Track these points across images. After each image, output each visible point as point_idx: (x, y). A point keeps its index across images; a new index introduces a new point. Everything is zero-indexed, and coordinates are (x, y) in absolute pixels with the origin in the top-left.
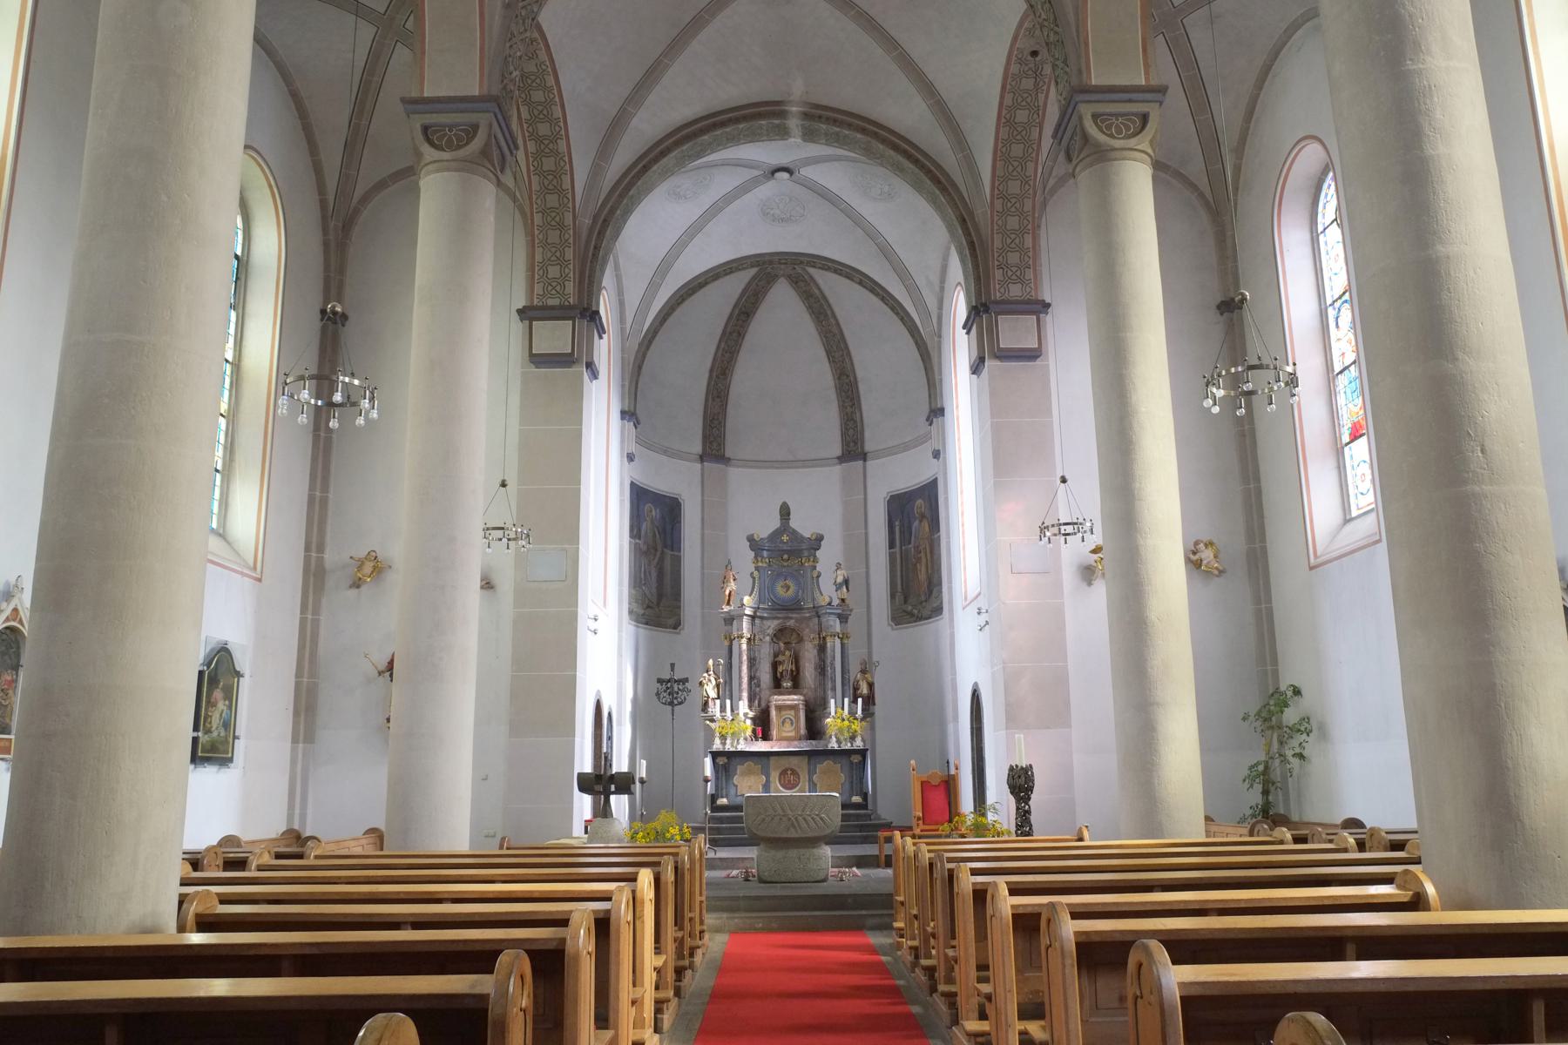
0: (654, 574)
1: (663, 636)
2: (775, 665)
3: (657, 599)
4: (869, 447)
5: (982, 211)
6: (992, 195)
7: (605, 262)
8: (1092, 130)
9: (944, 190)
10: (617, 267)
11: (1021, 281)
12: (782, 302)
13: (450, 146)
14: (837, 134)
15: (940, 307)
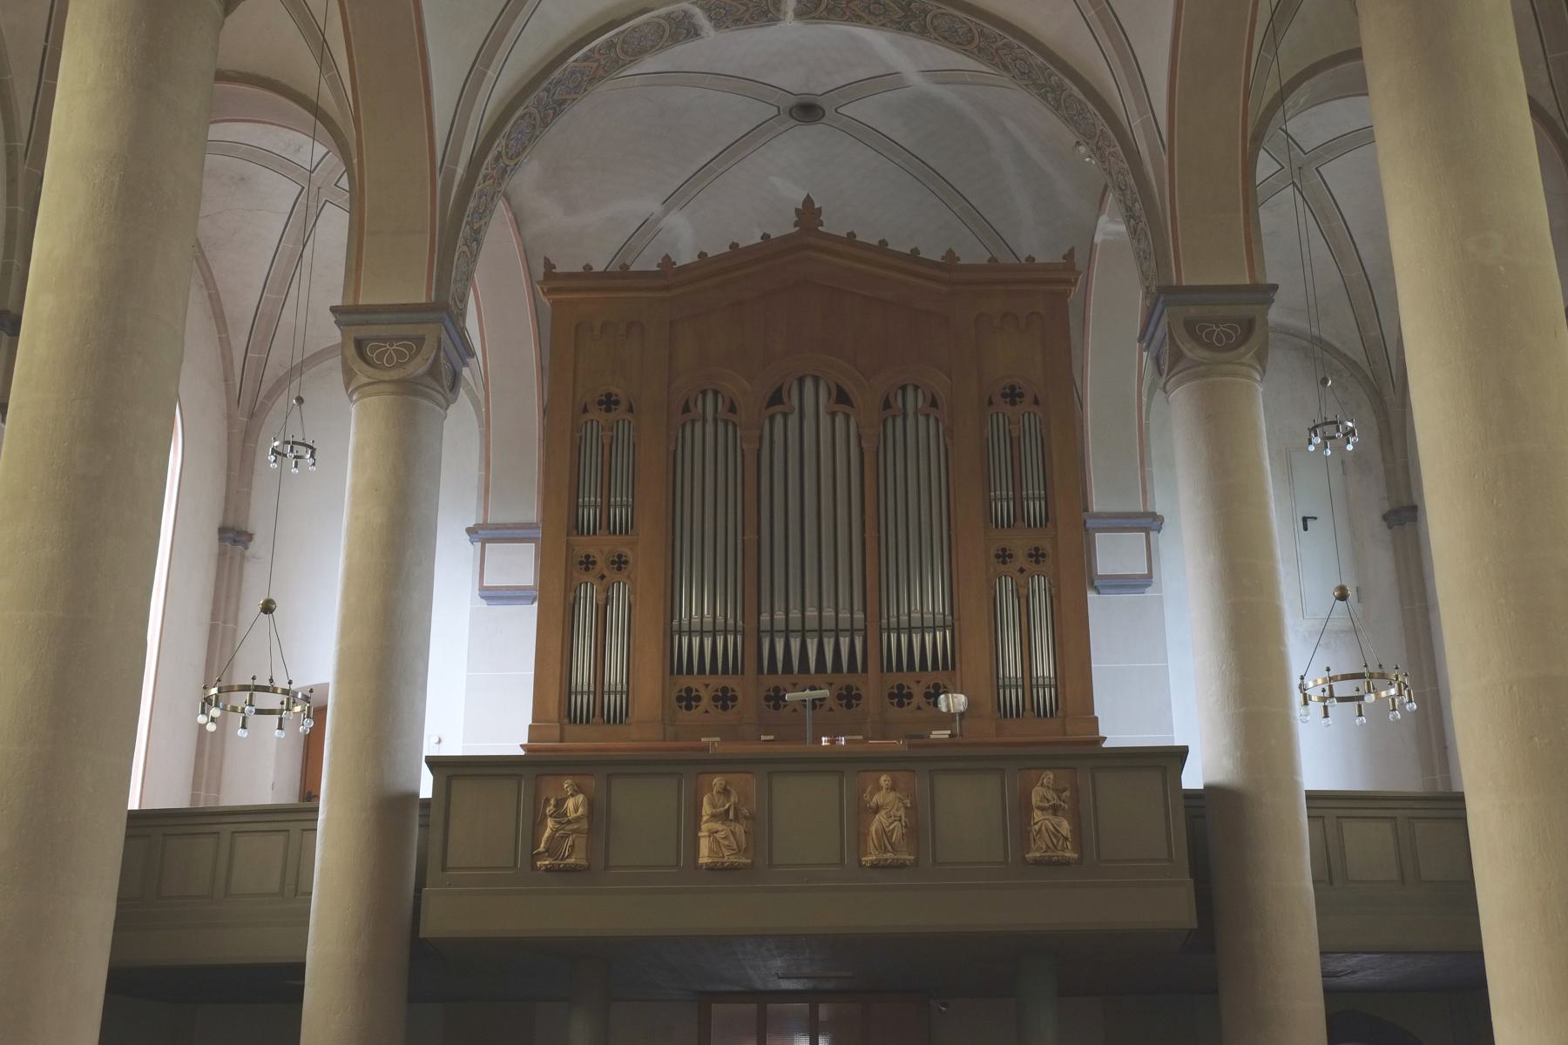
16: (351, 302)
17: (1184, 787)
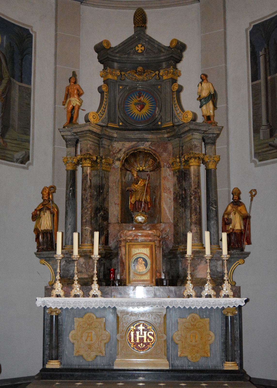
2: (126, 194)
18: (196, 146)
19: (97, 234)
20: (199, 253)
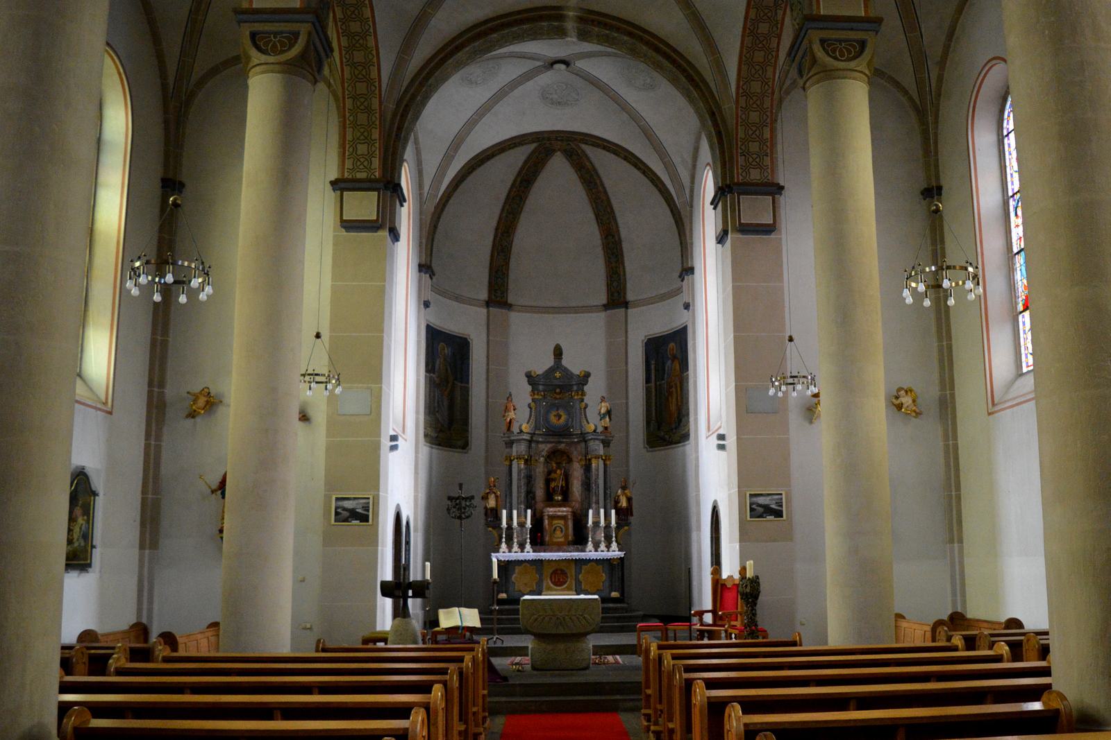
0: (446, 403)
1: (455, 456)
2: (548, 481)
3: (447, 421)
4: (630, 296)
5: (728, 107)
6: (737, 93)
7: (408, 134)
8: (820, 54)
9: (696, 86)
10: (416, 142)
11: (760, 167)
12: (558, 170)
13: (275, 51)
14: (607, 36)
15: (693, 182)
16: (340, 177)
17: (476, 611)
18: (596, 450)
19: (529, 511)
20: (596, 524)
